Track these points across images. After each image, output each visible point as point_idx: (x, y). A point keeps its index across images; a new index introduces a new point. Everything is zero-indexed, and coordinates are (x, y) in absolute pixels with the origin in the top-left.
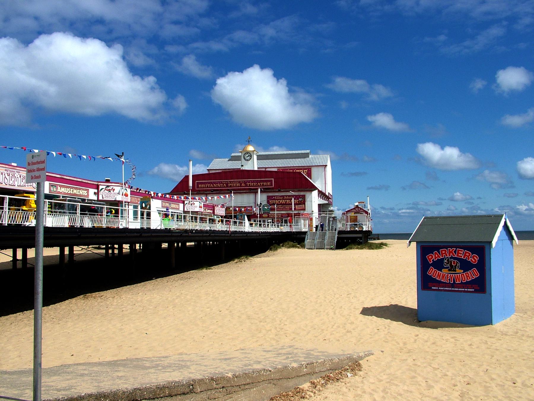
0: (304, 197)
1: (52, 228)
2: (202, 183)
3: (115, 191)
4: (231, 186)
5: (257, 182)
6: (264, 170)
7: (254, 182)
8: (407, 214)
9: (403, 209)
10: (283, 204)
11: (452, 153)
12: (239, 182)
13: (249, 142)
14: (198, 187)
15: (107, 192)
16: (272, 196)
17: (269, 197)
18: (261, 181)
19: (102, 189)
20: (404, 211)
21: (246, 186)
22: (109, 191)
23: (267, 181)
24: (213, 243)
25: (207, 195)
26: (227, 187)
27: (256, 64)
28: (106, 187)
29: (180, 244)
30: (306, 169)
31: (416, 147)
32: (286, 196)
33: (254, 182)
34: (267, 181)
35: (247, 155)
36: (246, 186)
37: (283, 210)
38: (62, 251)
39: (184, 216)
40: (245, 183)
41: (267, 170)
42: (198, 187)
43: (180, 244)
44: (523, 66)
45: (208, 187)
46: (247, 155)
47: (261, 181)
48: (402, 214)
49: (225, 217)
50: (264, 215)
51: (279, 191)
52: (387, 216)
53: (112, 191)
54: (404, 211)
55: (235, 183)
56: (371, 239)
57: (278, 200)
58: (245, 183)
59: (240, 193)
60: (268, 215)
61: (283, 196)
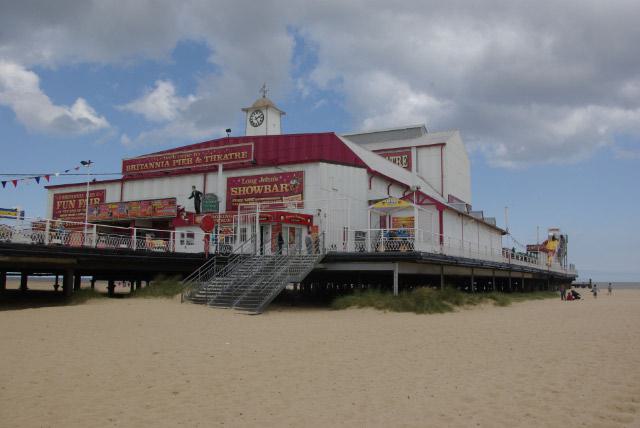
0: (300, 175)
21: (204, 161)
38: (132, 287)
40: (202, 156)
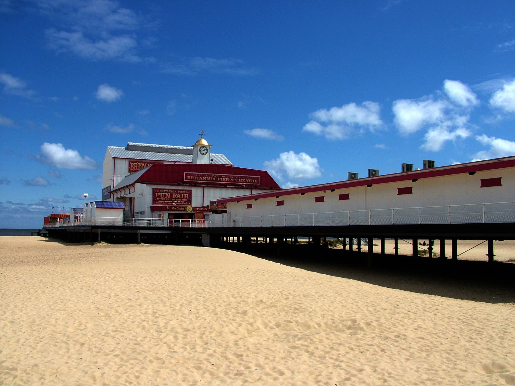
4: (220, 181)
5: (246, 178)
6: (173, 163)
7: (242, 178)
8: (37, 210)
9: (33, 205)
11: (72, 154)
12: (229, 177)
13: (202, 136)
14: (186, 179)
17: (154, 191)
18: (249, 178)
20: (34, 207)
21: (235, 181)
23: (254, 178)
24: (280, 240)
25: (204, 187)
26: (217, 180)
27: (444, 80)
29: (241, 238)
30: (149, 163)
31: (42, 144)
33: (242, 178)
34: (254, 178)
35: (204, 149)
36: (235, 181)
40: (234, 178)
42: (186, 179)
43: (241, 238)
45: (196, 180)
46: (204, 149)
47: (249, 178)
48: (32, 210)
52: (16, 211)
54: (34, 207)
55: (225, 178)
56: (450, 242)
58: (234, 178)
59: (232, 188)
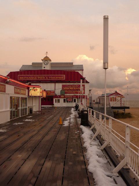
1: (44, 70)
2: (22, 76)
3: (37, 91)
10: (72, 90)
14: (19, 78)
15: (34, 91)
16: (65, 85)
19: (31, 89)
21: (49, 78)
22: (35, 90)
28: (33, 88)
32: (74, 85)
33: (53, 76)
36: (49, 78)
37: (72, 93)
39: (58, 100)
40: (48, 77)
41: (76, 71)
42: (19, 78)
44: (86, 169)
49: (90, 107)
50: (62, 96)
51: (69, 82)
53: (36, 91)
57: (68, 87)
60: (64, 96)
61: (72, 85)
